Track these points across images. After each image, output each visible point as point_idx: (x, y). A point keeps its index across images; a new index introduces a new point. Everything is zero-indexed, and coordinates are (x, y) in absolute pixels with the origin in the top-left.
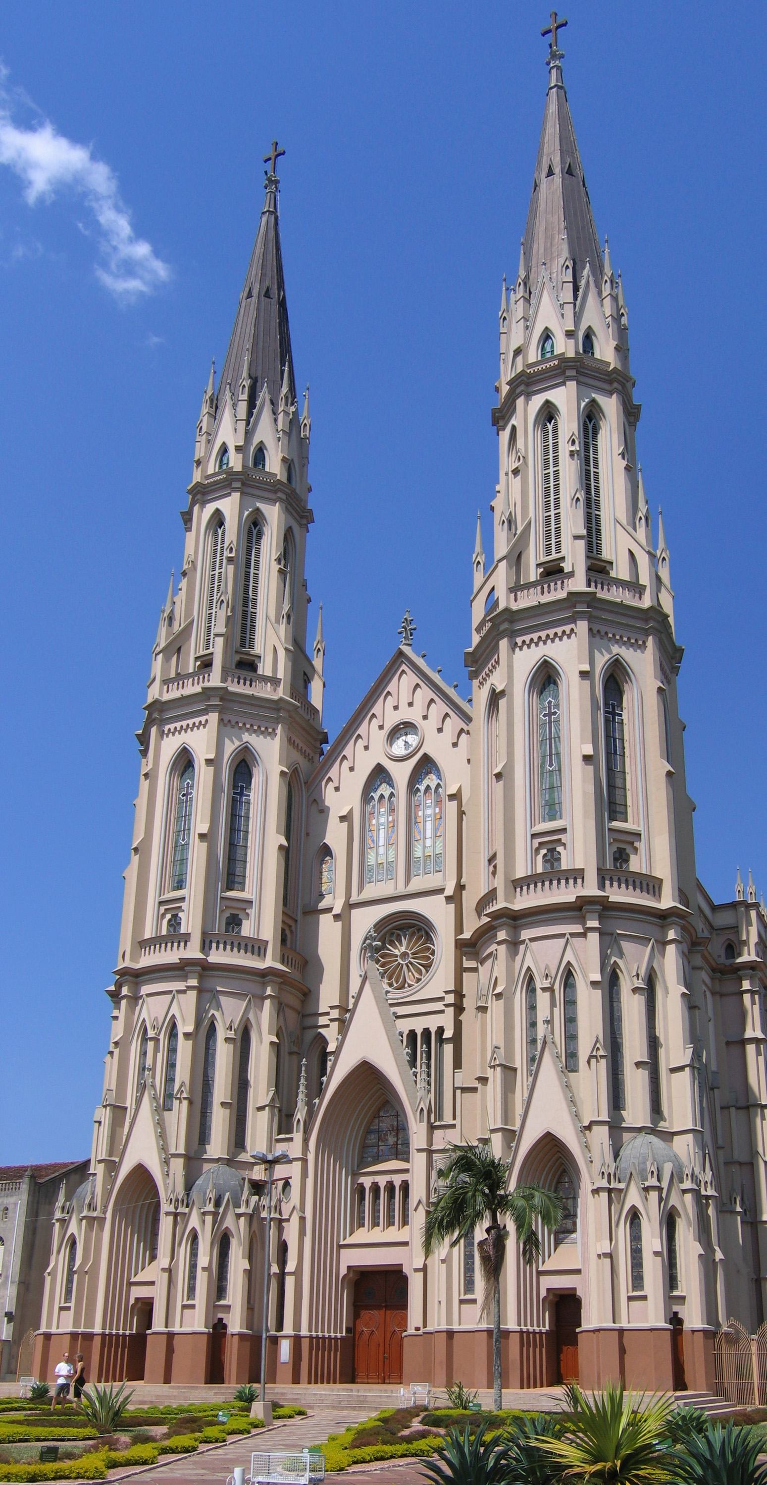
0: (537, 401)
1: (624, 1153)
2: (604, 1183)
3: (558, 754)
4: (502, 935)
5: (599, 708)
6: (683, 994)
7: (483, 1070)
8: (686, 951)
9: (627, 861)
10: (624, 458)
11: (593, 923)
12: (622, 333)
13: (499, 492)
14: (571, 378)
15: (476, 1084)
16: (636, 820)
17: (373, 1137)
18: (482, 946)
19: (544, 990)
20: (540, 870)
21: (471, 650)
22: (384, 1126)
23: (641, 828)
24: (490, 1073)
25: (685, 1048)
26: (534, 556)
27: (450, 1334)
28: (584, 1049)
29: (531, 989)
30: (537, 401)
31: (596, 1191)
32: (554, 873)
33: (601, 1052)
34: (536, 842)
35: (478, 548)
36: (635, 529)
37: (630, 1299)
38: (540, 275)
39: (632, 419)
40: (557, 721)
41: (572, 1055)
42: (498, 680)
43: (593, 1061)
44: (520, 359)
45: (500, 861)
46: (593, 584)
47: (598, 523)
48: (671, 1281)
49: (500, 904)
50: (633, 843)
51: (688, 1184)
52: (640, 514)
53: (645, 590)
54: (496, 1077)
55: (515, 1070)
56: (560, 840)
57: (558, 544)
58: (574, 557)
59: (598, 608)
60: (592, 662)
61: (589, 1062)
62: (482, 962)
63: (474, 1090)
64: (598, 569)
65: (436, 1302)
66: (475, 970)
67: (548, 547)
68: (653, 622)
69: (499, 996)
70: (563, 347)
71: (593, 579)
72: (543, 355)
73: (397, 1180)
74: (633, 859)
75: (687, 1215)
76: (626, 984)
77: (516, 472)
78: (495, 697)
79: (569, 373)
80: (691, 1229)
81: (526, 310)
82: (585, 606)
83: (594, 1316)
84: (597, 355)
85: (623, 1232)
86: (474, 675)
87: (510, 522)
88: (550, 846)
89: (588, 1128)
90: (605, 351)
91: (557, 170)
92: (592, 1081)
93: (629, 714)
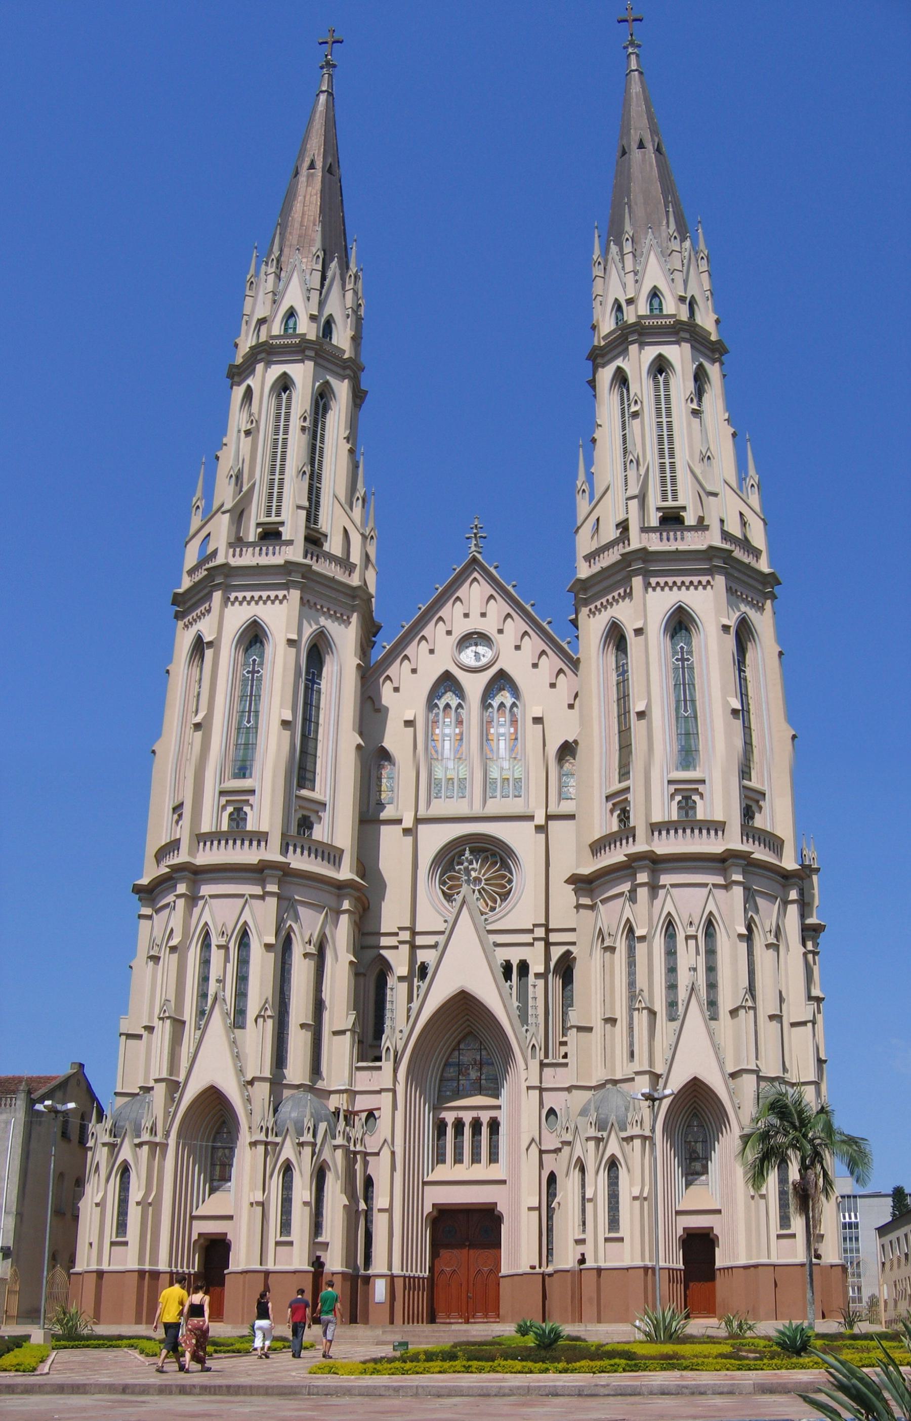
0: (276, 371)
1: (285, 1109)
2: (262, 1137)
3: (257, 712)
4: (182, 888)
5: (300, 676)
6: (351, 963)
7: (151, 1018)
8: (358, 920)
9: (311, 828)
10: (348, 442)
11: (273, 888)
12: (359, 323)
13: (226, 445)
14: (309, 358)
15: (142, 1032)
16: (323, 791)
18: (162, 892)
19: (219, 947)
20: (225, 827)
21: (181, 591)
22: (466, 1058)
23: (327, 799)
24: (156, 1023)
25: (348, 1014)
26: (256, 515)
27: (100, 1274)
28: (253, 1007)
29: (206, 944)
30: (276, 371)
31: (254, 1144)
32: (238, 831)
33: (269, 1013)
34: (223, 800)
35: (199, 494)
36: (351, 509)
37: (278, 1244)
38: (292, 258)
39: (358, 401)
40: (260, 679)
41: (240, 1012)
42: (206, 627)
43: (260, 1020)
44: (264, 328)
45: (187, 811)
46: (309, 556)
47: (318, 496)
48: (317, 1226)
49: (182, 857)
50: (317, 812)
51: (339, 1141)
52: (358, 495)
53: (355, 568)
54: (164, 1030)
55: (184, 1023)
56: (248, 801)
57: (279, 507)
58: (293, 526)
59: (313, 580)
60: (300, 632)
61: (256, 1021)
62: (158, 911)
63: (139, 1037)
64: (314, 540)
65: (87, 1245)
66: (150, 917)
67: (269, 507)
68: (355, 600)
69: (173, 949)
70: (306, 328)
71: (310, 551)
72: (286, 329)
74: (316, 827)
75: (337, 1171)
76: (298, 950)
77: (248, 433)
78: (199, 646)
79: (308, 353)
80: (339, 1182)
81: (276, 285)
82: (300, 575)
83: (241, 1258)
84: (334, 341)
85: (276, 1183)
86: (179, 616)
87: (237, 477)
88: (237, 804)
89: (251, 1083)
90: (342, 338)
91: (319, 164)
92: (257, 1039)
93: (327, 684)
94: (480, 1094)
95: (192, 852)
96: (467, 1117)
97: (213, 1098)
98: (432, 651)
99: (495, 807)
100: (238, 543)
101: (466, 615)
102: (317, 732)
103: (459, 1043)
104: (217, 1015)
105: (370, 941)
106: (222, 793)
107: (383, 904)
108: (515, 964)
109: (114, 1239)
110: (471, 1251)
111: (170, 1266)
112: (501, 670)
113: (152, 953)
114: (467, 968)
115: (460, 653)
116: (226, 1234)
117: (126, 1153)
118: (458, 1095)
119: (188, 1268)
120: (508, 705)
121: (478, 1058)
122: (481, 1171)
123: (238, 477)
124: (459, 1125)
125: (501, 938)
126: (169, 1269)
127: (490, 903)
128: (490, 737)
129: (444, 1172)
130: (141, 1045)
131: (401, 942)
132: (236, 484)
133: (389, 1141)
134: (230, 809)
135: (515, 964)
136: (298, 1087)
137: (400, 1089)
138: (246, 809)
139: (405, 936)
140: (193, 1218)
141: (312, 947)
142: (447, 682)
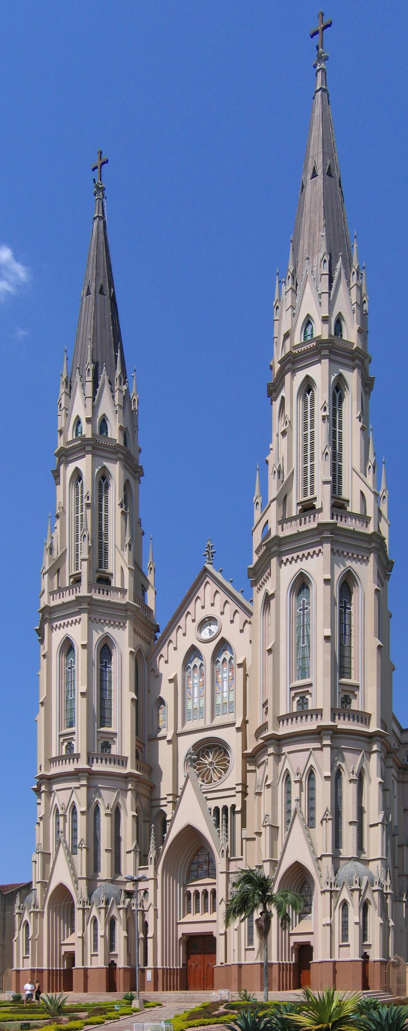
1: (341, 871)
2: (328, 888)
4: (271, 750)
5: (336, 605)
6: (380, 783)
7: (259, 828)
8: (383, 757)
11: (327, 742)
17: (195, 866)
19: (296, 782)
20: (64, 753)
22: (201, 860)
23: (359, 683)
24: (263, 830)
26: (296, 497)
27: (240, 966)
28: (319, 814)
29: (58, 816)
31: (323, 892)
32: (71, 756)
33: (329, 817)
34: (62, 739)
41: (311, 819)
43: (324, 822)
46: (335, 517)
47: (340, 472)
48: (364, 936)
50: (354, 692)
51: (376, 887)
52: (370, 464)
53: (370, 520)
54: (266, 832)
55: (278, 828)
56: (308, 691)
60: (332, 573)
61: (322, 822)
63: (254, 839)
64: (339, 506)
65: (232, 950)
69: (268, 786)
71: (335, 513)
73: (209, 888)
75: (375, 903)
80: (377, 910)
83: (320, 954)
85: (338, 913)
87: (279, 472)
88: (301, 695)
89: (320, 858)
92: (323, 834)
93: (114, 666)
94: (209, 877)
95: (47, 769)
96: (200, 889)
97: (62, 889)
98: (184, 635)
99: (218, 721)
100: (282, 522)
101: (203, 607)
102: (110, 695)
103: (198, 852)
104: (297, 822)
105: (155, 803)
106: (61, 736)
107: (162, 783)
108: (221, 808)
109: (24, 956)
110: (205, 956)
111: (278, 960)
112: (222, 638)
113: (257, 791)
114: (189, 813)
115: (200, 633)
116: (310, 942)
117: (26, 917)
118: (197, 878)
119: (289, 961)
120: (228, 659)
121: (207, 858)
122: (207, 916)
123: (280, 472)
124: (197, 893)
125: (210, 796)
126: (277, 962)
127: (219, 775)
128: (219, 681)
129: (189, 918)
130: (256, 842)
131: (168, 802)
132: (279, 477)
133: (153, 903)
134: (66, 744)
135: (221, 808)
136: (105, 880)
137: (159, 878)
138: (73, 742)
139: (170, 798)
140: (290, 935)
141: (354, 775)
142: (193, 652)
